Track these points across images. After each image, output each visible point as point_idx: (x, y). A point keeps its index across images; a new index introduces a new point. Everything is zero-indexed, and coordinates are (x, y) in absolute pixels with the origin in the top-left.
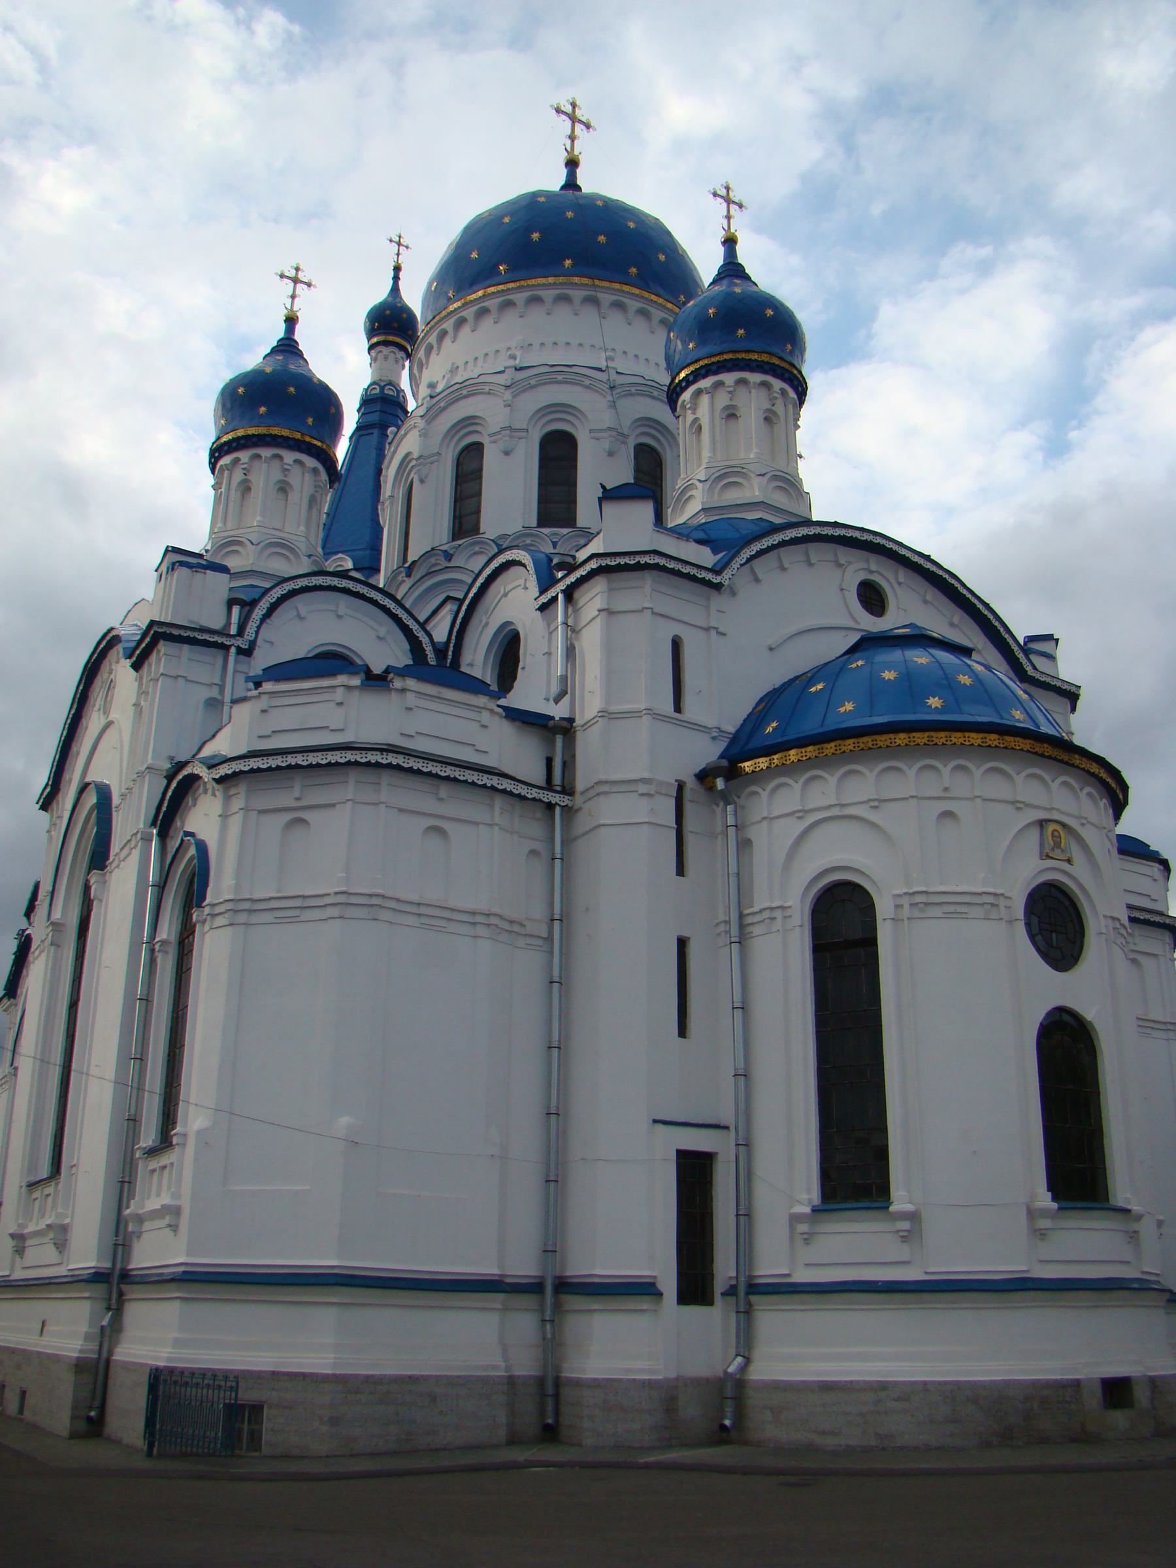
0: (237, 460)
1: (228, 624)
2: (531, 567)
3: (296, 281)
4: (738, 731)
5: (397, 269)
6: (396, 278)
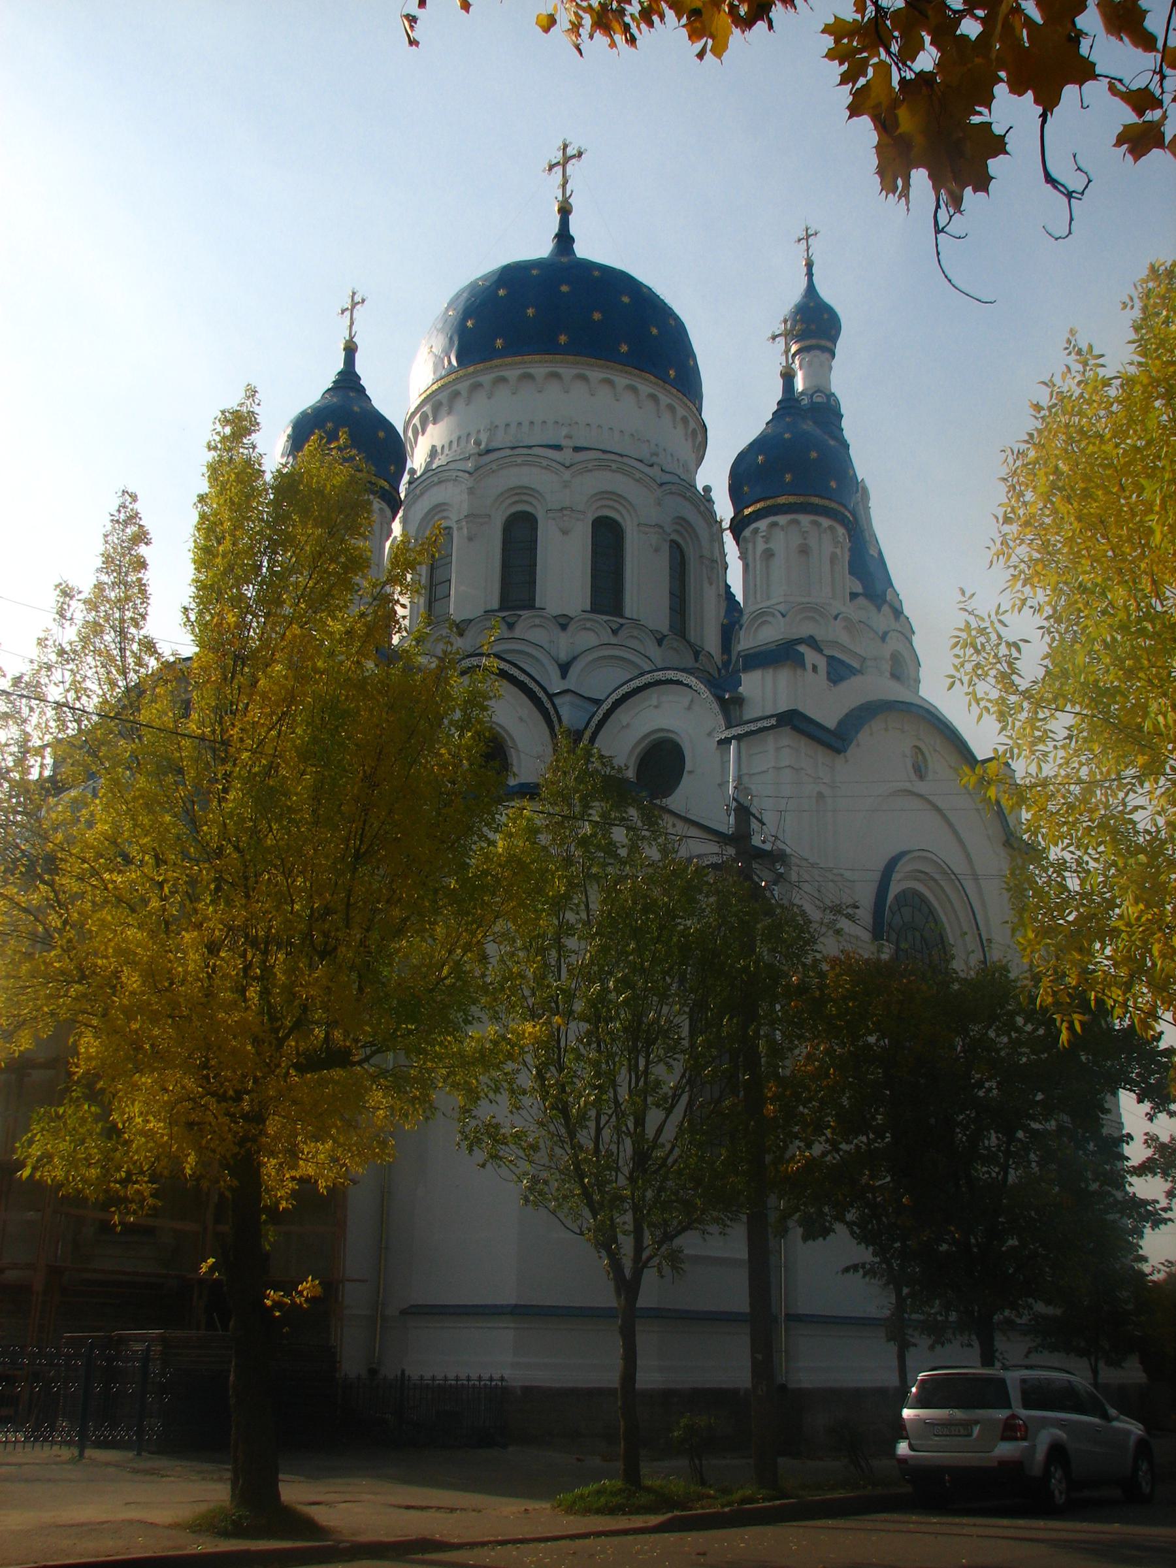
0: (756, 531)
5: (809, 265)
6: (810, 274)
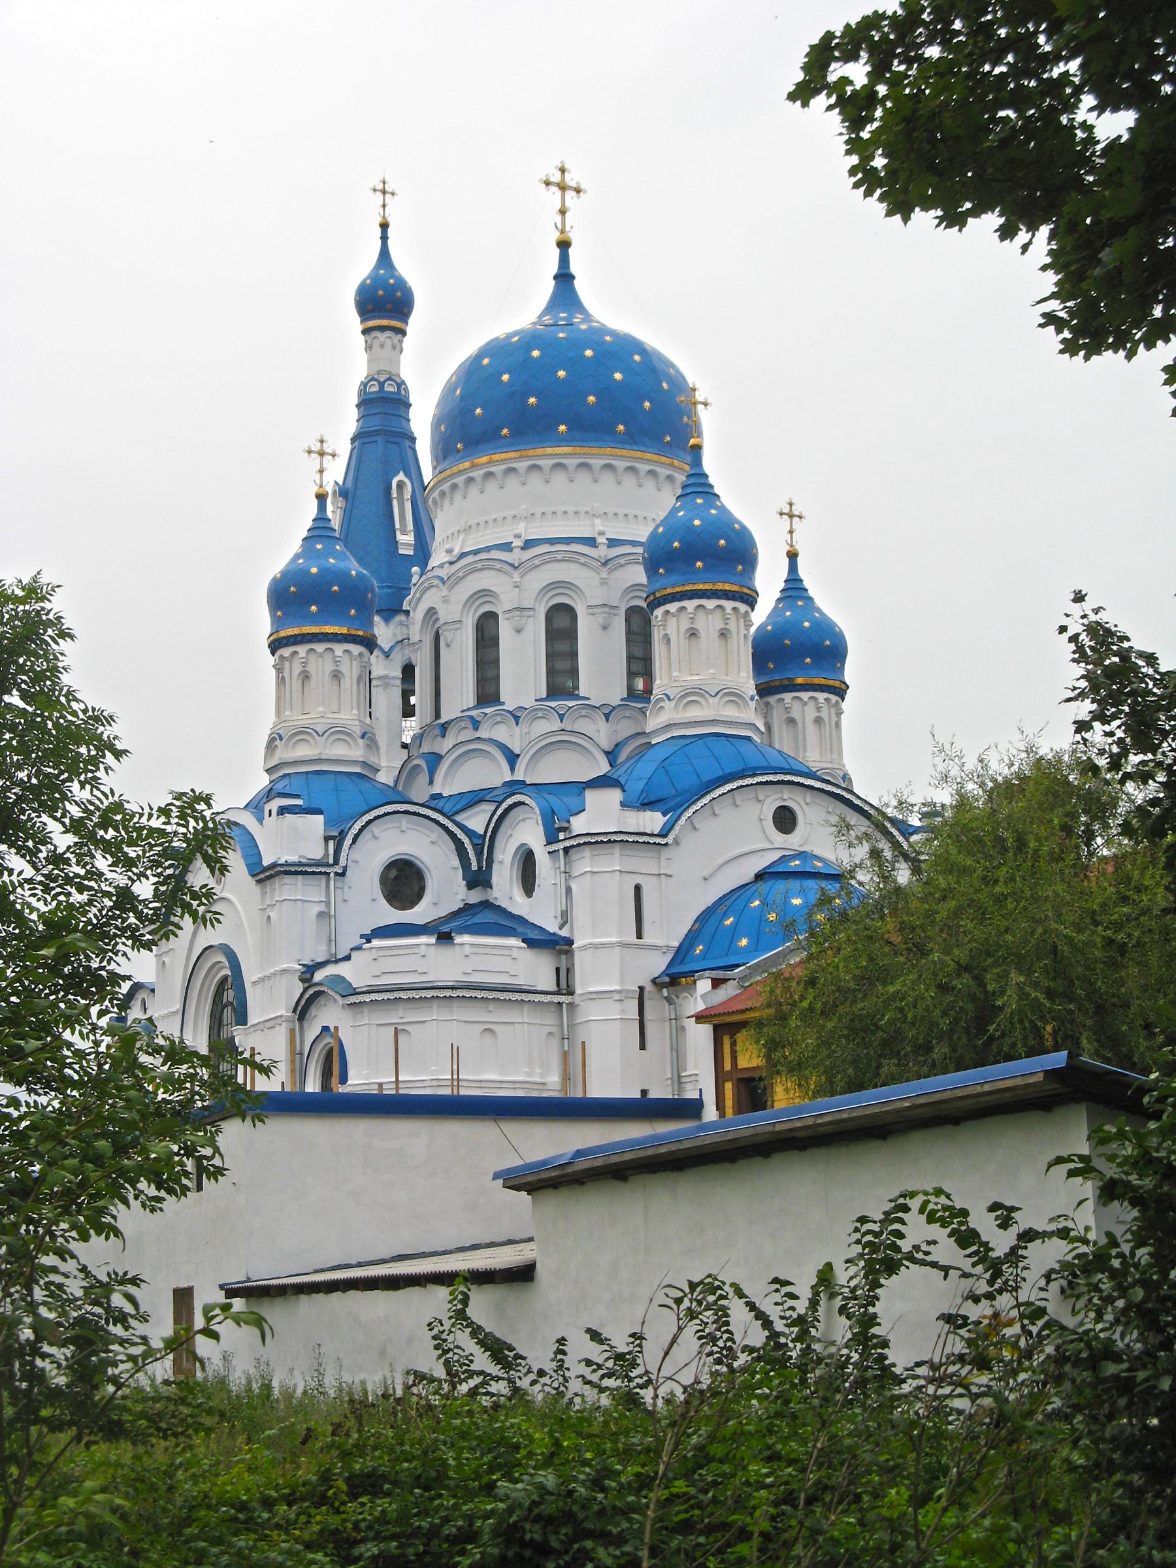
1: (326, 854)
2: (537, 810)
3: (322, 454)
4: (681, 945)
5: (384, 226)
6: (384, 238)
